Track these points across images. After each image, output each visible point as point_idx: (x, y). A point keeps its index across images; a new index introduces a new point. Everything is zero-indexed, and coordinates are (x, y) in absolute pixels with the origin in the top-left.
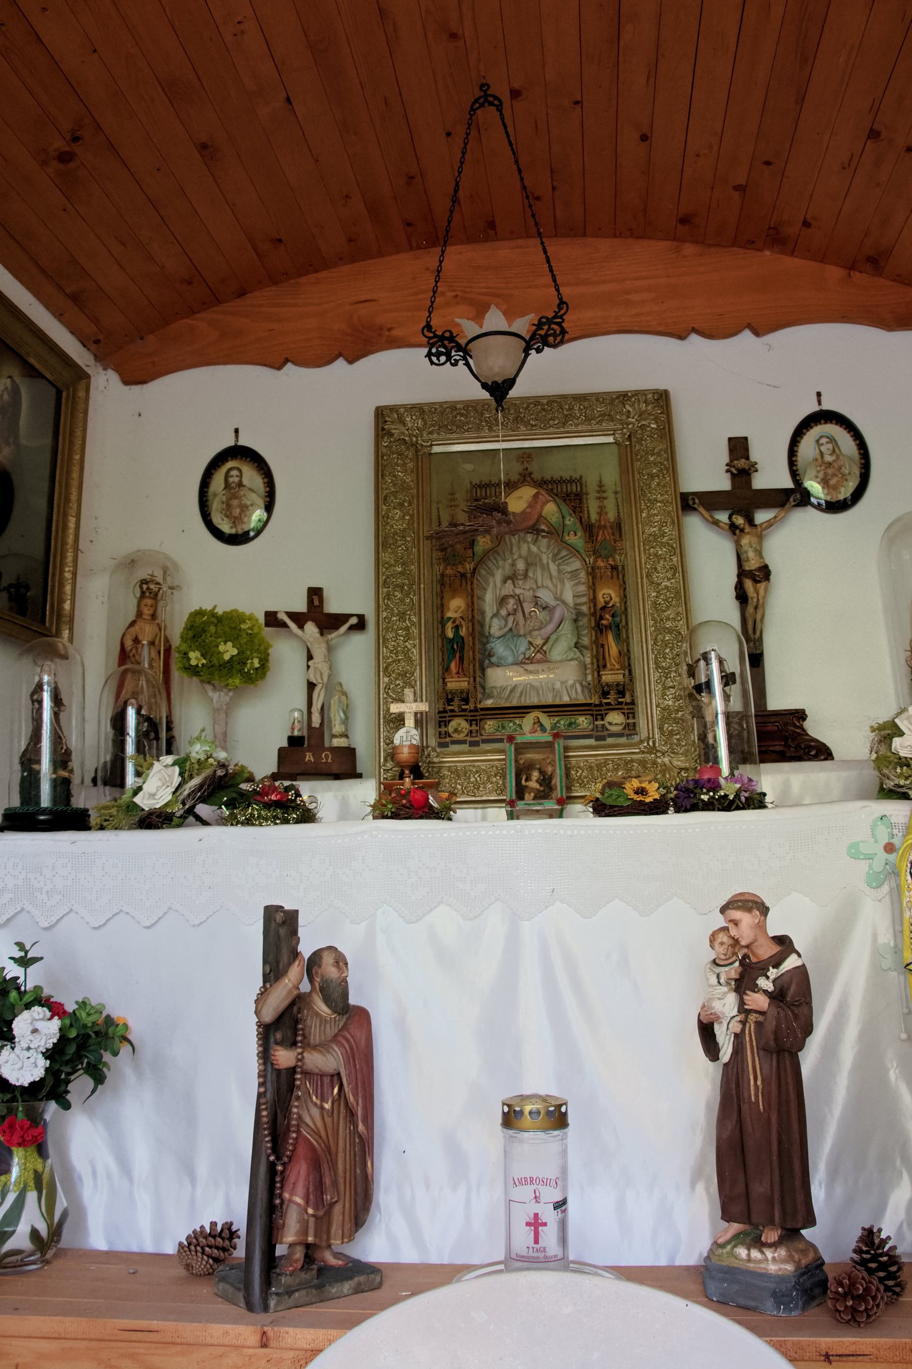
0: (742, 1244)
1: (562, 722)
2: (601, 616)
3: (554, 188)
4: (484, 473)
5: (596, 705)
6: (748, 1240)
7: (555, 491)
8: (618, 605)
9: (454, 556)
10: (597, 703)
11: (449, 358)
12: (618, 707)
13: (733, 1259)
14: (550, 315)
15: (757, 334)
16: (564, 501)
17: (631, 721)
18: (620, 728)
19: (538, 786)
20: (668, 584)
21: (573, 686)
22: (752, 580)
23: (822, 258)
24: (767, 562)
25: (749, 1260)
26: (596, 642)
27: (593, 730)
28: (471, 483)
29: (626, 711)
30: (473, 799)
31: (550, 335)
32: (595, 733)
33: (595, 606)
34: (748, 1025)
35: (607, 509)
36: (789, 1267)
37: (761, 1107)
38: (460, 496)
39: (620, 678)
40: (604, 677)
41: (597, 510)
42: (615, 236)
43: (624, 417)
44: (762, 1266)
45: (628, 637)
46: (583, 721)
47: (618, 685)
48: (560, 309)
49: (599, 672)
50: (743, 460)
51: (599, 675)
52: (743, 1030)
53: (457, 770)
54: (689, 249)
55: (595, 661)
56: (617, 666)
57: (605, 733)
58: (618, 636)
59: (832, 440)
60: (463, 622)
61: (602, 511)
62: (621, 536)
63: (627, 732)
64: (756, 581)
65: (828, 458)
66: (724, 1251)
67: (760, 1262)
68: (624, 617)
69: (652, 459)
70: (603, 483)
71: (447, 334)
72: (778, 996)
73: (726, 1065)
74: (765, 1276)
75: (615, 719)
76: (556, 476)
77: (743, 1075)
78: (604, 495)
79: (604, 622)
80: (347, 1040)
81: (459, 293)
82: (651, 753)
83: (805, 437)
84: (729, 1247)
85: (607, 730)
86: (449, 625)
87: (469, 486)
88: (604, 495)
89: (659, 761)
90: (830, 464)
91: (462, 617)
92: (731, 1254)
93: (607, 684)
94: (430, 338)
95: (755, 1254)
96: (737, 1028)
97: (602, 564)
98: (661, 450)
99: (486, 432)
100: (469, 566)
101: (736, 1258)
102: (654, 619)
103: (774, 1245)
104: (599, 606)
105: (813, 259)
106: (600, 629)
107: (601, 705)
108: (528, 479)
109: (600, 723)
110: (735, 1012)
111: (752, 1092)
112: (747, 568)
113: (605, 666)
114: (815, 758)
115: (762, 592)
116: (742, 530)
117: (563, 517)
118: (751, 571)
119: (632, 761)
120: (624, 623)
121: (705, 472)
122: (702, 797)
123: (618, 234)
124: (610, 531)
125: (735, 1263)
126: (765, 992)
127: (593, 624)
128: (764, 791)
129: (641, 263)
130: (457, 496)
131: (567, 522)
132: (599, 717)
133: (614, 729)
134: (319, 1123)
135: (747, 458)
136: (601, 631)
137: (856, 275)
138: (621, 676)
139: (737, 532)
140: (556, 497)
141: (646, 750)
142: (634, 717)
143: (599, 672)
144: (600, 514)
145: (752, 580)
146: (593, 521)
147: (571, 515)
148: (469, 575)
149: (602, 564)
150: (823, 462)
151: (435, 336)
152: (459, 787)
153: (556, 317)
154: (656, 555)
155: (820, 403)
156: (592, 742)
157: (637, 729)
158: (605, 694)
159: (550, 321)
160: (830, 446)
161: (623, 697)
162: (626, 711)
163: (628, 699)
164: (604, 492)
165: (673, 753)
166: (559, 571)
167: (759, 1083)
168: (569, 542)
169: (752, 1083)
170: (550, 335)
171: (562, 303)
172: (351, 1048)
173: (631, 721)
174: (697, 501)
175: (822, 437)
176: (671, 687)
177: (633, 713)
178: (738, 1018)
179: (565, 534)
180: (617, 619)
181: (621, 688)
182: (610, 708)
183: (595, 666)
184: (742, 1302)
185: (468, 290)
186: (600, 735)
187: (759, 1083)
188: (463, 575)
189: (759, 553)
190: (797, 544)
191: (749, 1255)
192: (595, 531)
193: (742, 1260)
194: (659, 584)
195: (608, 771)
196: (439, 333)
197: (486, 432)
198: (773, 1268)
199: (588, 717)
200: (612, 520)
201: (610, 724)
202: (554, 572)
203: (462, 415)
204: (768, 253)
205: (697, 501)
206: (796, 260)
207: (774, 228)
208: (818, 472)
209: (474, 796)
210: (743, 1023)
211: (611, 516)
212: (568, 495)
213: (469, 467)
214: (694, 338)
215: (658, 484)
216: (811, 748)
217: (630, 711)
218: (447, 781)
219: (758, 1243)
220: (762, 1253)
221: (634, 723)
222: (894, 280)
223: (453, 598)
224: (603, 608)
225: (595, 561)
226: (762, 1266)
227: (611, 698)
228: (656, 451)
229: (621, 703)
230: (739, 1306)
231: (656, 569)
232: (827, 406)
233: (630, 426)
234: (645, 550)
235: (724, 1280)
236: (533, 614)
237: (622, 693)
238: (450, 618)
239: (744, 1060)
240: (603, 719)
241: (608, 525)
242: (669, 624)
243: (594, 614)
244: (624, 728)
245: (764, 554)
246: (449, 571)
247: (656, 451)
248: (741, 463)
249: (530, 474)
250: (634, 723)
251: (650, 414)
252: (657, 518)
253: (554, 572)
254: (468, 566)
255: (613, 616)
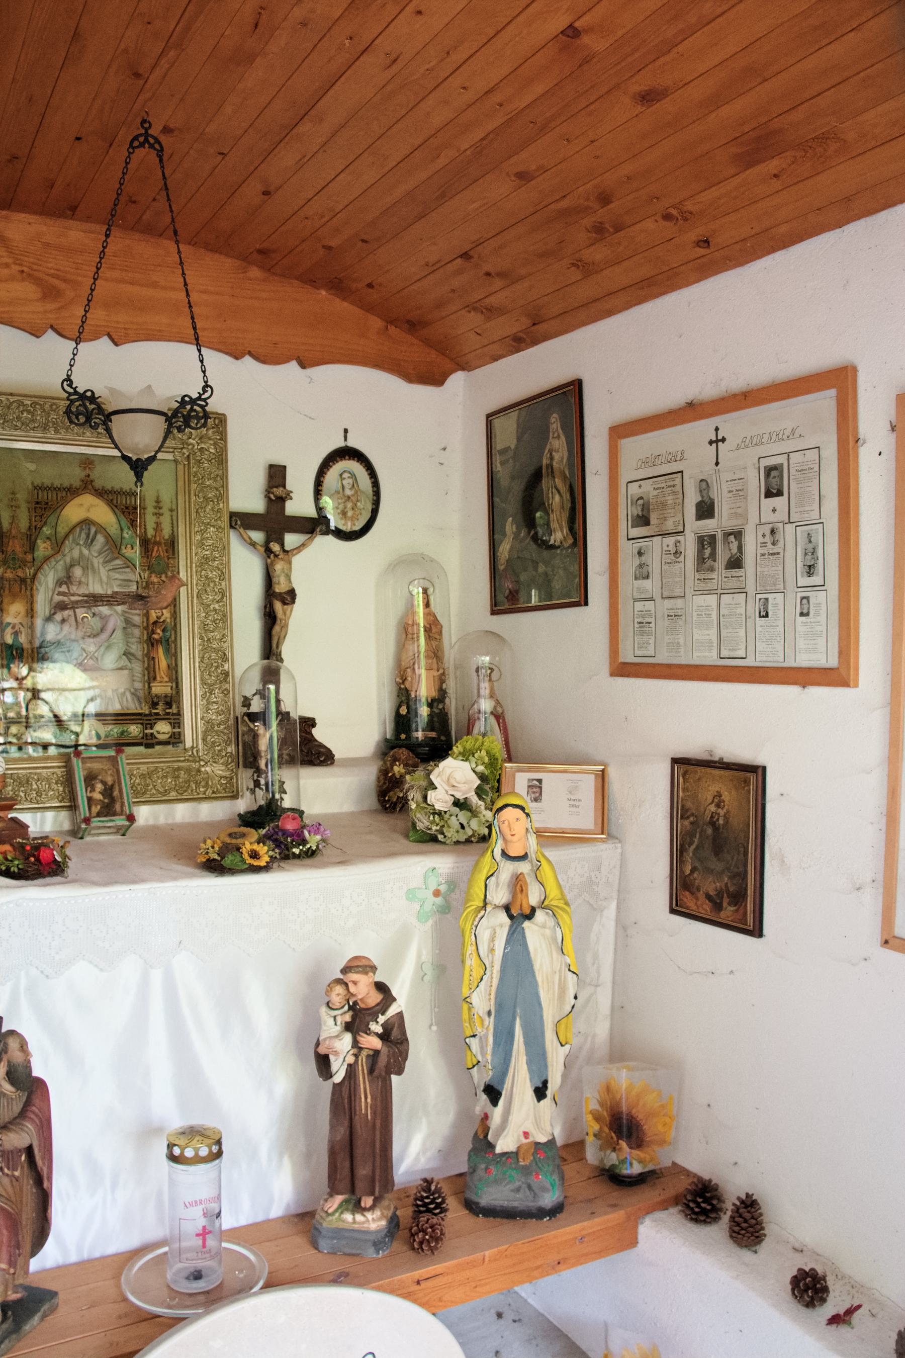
0: (347, 1210)
1: (115, 730)
2: (153, 630)
3: (154, 200)
4: (50, 475)
5: (146, 715)
6: (351, 1207)
7: (115, 502)
8: (168, 620)
9: (14, 559)
10: (147, 712)
11: (88, 419)
12: (166, 717)
13: (340, 1223)
14: (195, 396)
15: (303, 366)
16: (123, 513)
17: (176, 730)
18: (167, 736)
19: (101, 797)
20: (217, 606)
21: (124, 694)
22: (276, 601)
23: (370, 308)
24: (294, 586)
25: (354, 1222)
26: (147, 655)
27: (143, 738)
28: (32, 483)
29: (172, 721)
30: (36, 806)
31: (193, 417)
32: (145, 741)
33: (148, 619)
34: (360, 1058)
35: (163, 526)
36: (383, 1223)
37: (369, 1117)
38: (22, 496)
39: (168, 690)
40: (153, 689)
41: (154, 526)
42: (189, 244)
43: (185, 437)
44: (365, 1225)
45: (176, 652)
46: (134, 730)
47: (166, 696)
48: (205, 391)
49: (149, 684)
50: (281, 489)
51: (150, 687)
52: (356, 1061)
53: (19, 778)
54: (255, 272)
55: (146, 672)
56: (166, 679)
57: (154, 741)
58: (167, 651)
59: (353, 476)
60: (22, 629)
61: (158, 527)
62: (174, 554)
63: (173, 740)
64: (284, 603)
65: (348, 492)
66: (334, 1218)
67: (364, 1223)
68: (173, 633)
69: (208, 483)
70: (161, 499)
71: (89, 394)
72: (385, 1037)
73: (335, 1085)
74: (367, 1232)
75: (163, 728)
76: (117, 487)
77: (355, 1096)
78: (161, 511)
79: (156, 636)
80: (33, 1112)
81: (25, 269)
82: (195, 762)
83: (331, 470)
84: (337, 1214)
85: (156, 738)
86: (9, 630)
87: (30, 487)
88: (161, 511)
89: (203, 769)
90: (349, 497)
91: (21, 623)
92: (340, 1219)
93: (156, 695)
94: (70, 394)
95: (359, 1217)
96: (351, 1059)
97: (156, 580)
98: (217, 476)
99: (51, 433)
100: (29, 572)
101: (343, 1221)
102: (201, 638)
103: (372, 1208)
104: (152, 620)
105: (361, 307)
106: (152, 643)
107: (150, 715)
108: (90, 487)
109: (149, 731)
110: (350, 1047)
111: (363, 1107)
112: (277, 591)
113: (155, 678)
114: (321, 764)
115: (288, 612)
116: (276, 556)
117: (122, 530)
118: (280, 593)
119: (179, 769)
120: (173, 638)
121: (246, 494)
122: (294, 850)
123: (193, 243)
124: (164, 548)
125: (341, 1225)
126: (377, 1034)
127: (145, 638)
128: (302, 808)
129: (211, 275)
130: (18, 496)
131: (125, 535)
132: (149, 726)
133: (161, 737)
134: (10, 1189)
135: (284, 487)
136: (153, 645)
137: (392, 329)
138: (169, 688)
139: (272, 556)
140: (116, 510)
141: (191, 759)
142: (179, 727)
143: (149, 684)
144: (156, 530)
145: (276, 601)
146: (149, 536)
147: (129, 528)
148: (29, 580)
149: (156, 580)
150: (344, 495)
151: (76, 393)
152: (22, 794)
153: (199, 398)
154: (207, 577)
155: (346, 439)
156: (141, 749)
157: (182, 738)
158: (154, 705)
159: (193, 402)
160: (351, 481)
161: (171, 708)
162: (172, 721)
163: (174, 710)
164: (160, 508)
165: (215, 762)
166: (108, 577)
167: (369, 1100)
168: (126, 555)
169: (363, 1100)
170: (193, 417)
171: (206, 386)
172: (40, 1119)
173: (176, 730)
174: (239, 522)
175: (345, 471)
176: (214, 702)
177: (179, 723)
178: (351, 1052)
179: (123, 547)
180: (168, 634)
181: (168, 700)
182: (158, 718)
183: (146, 678)
184: (347, 1250)
185: (35, 267)
186: (149, 742)
187: (369, 1100)
188: (23, 581)
189: (288, 577)
190: (315, 565)
191: (354, 1219)
192: (151, 546)
193: (348, 1223)
194: (209, 606)
195: (158, 777)
196: (81, 390)
197: (51, 433)
198: (373, 1226)
199: (139, 726)
200: (166, 537)
201: (158, 732)
202: (105, 579)
203: (29, 412)
204: (324, 293)
205: (239, 522)
206: (346, 304)
207: (340, 279)
208: (339, 504)
209: (37, 803)
210: (356, 1056)
211: (166, 532)
212: (127, 508)
213: (32, 466)
214: (248, 359)
215: (213, 509)
216: (319, 754)
217: (176, 720)
218: (10, 788)
219: (358, 1207)
220: (364, 1216)
221: (179, 733)
222: (423, 342)
223: (12, 603)
224: (155, 623)
225: (150, 577)
226: (365, 1225)
227: (160, 709)
228: (212, 476)
229: (168, 714)
230: (345, 1254)
231: (206, 591)
232: (352, 443)
233: (190, 447)
234: (197, 571)
235: (333, 1238)
236: (85, 620)
237: (169, 704)
238: (9, 624)
239: (356, 1085)
240: (152, 728)
241: (163, 541)
242: (215, 645)
243: (146, 628)
244: (171, 737)
245: (292, 579)
246: (9, 575)
247: (212, 476)
248: (279, 491)
249: (92, 481)
250: (179, 733)
251: (210, 439)
252: (210, 542)
253: (105, 579)
254: (28, 571)
255: (164, 631)
